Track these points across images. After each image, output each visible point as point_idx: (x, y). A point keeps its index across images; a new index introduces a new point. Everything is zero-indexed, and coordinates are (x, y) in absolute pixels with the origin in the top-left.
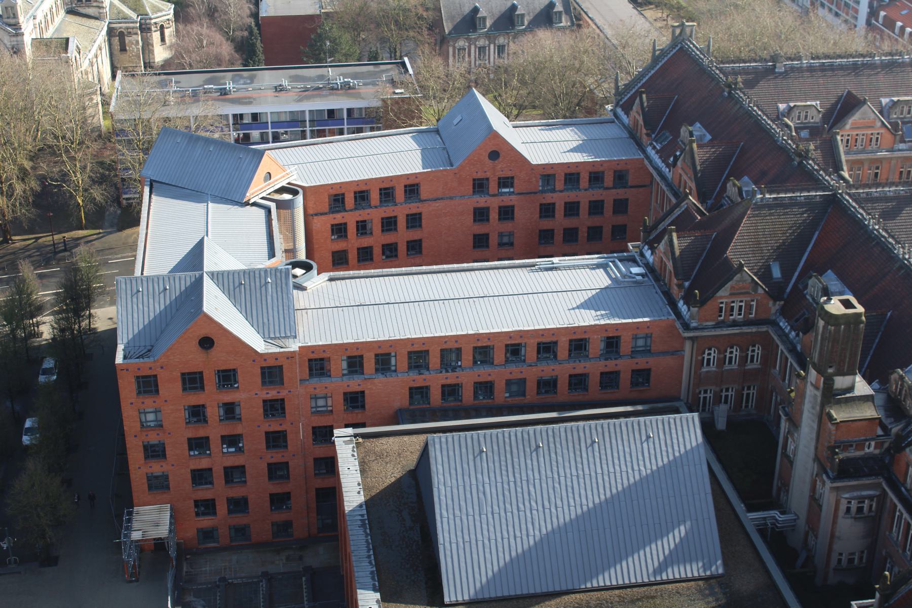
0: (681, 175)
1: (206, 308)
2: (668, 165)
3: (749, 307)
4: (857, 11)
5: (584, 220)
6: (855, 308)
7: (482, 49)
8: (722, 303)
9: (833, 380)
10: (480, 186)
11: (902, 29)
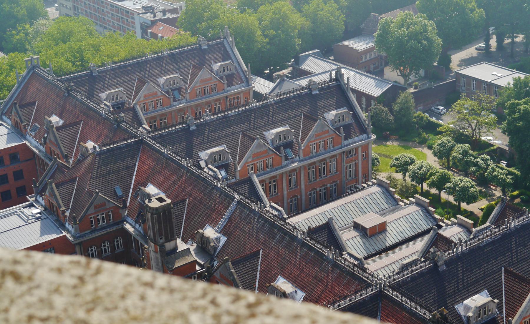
0: (50, 148)
1: (368, 227)
2: (41, 144)
3: (108, 216)
6: (166, 201)
8: (91, 218)
9: (164, 246)
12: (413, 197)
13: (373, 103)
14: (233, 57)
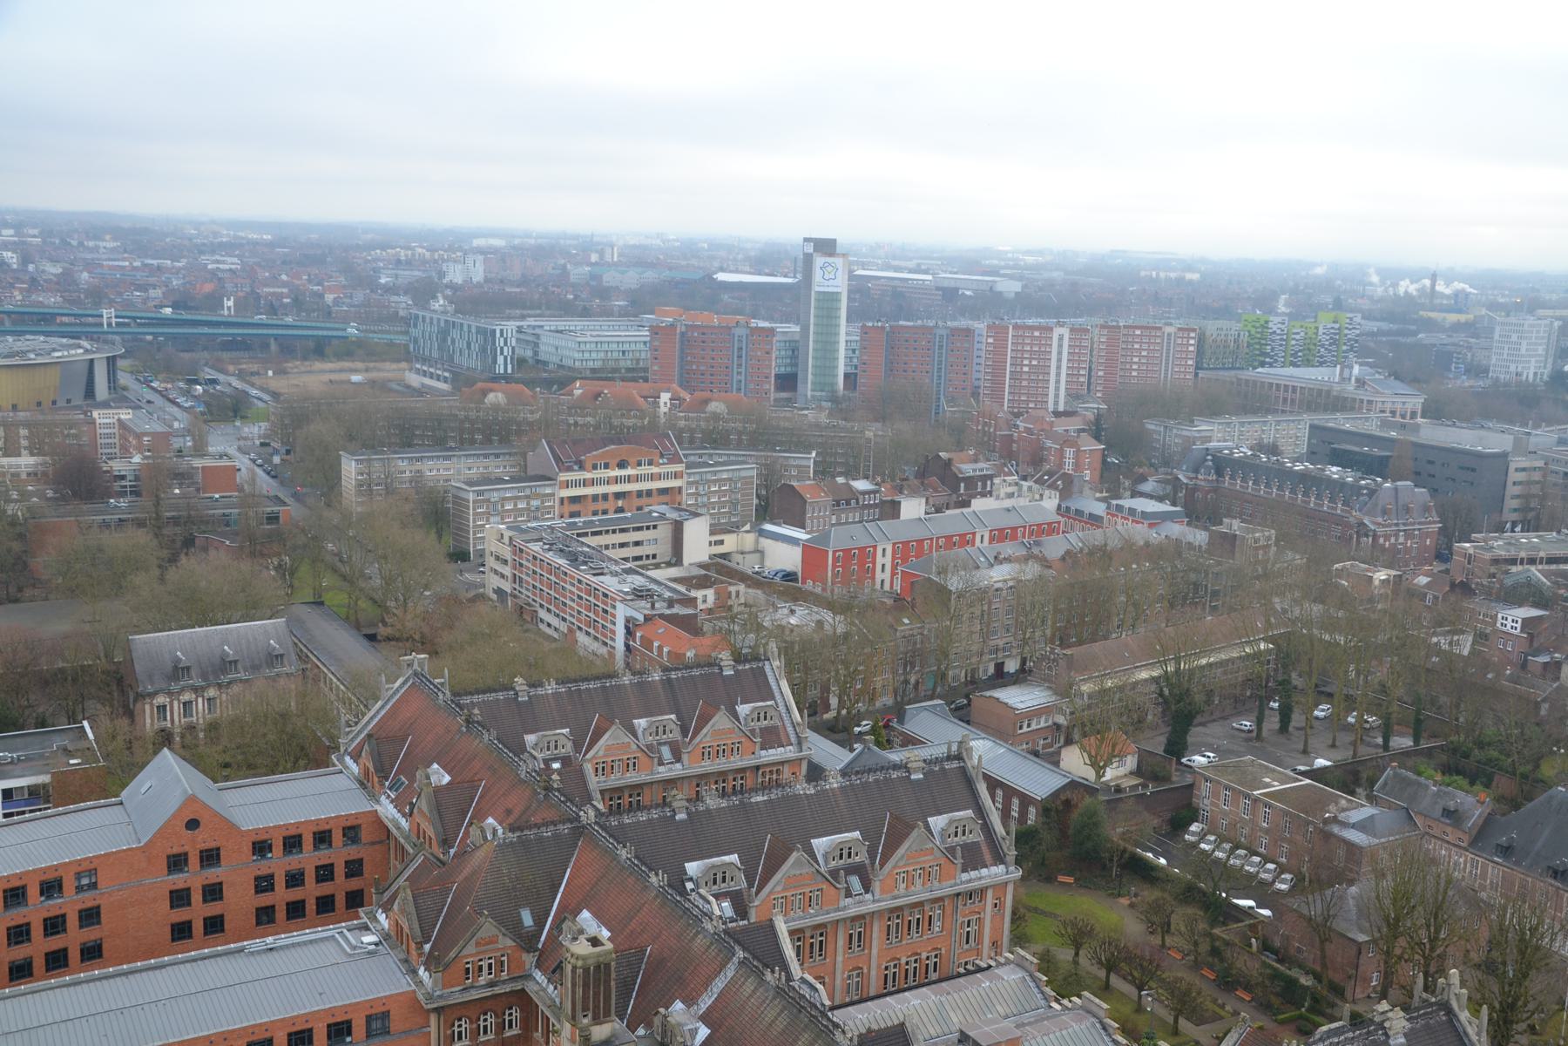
2: (404, 815)
4: (613, 632)
5: (311, 890)
7: (187, 704)
10: (177, 862)
11: (660, 648)
12: (1079, 996)
13: (1032, 810)
14: (777, 694)
